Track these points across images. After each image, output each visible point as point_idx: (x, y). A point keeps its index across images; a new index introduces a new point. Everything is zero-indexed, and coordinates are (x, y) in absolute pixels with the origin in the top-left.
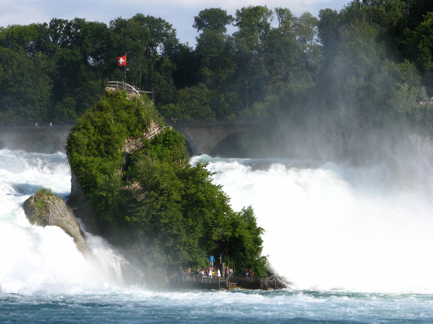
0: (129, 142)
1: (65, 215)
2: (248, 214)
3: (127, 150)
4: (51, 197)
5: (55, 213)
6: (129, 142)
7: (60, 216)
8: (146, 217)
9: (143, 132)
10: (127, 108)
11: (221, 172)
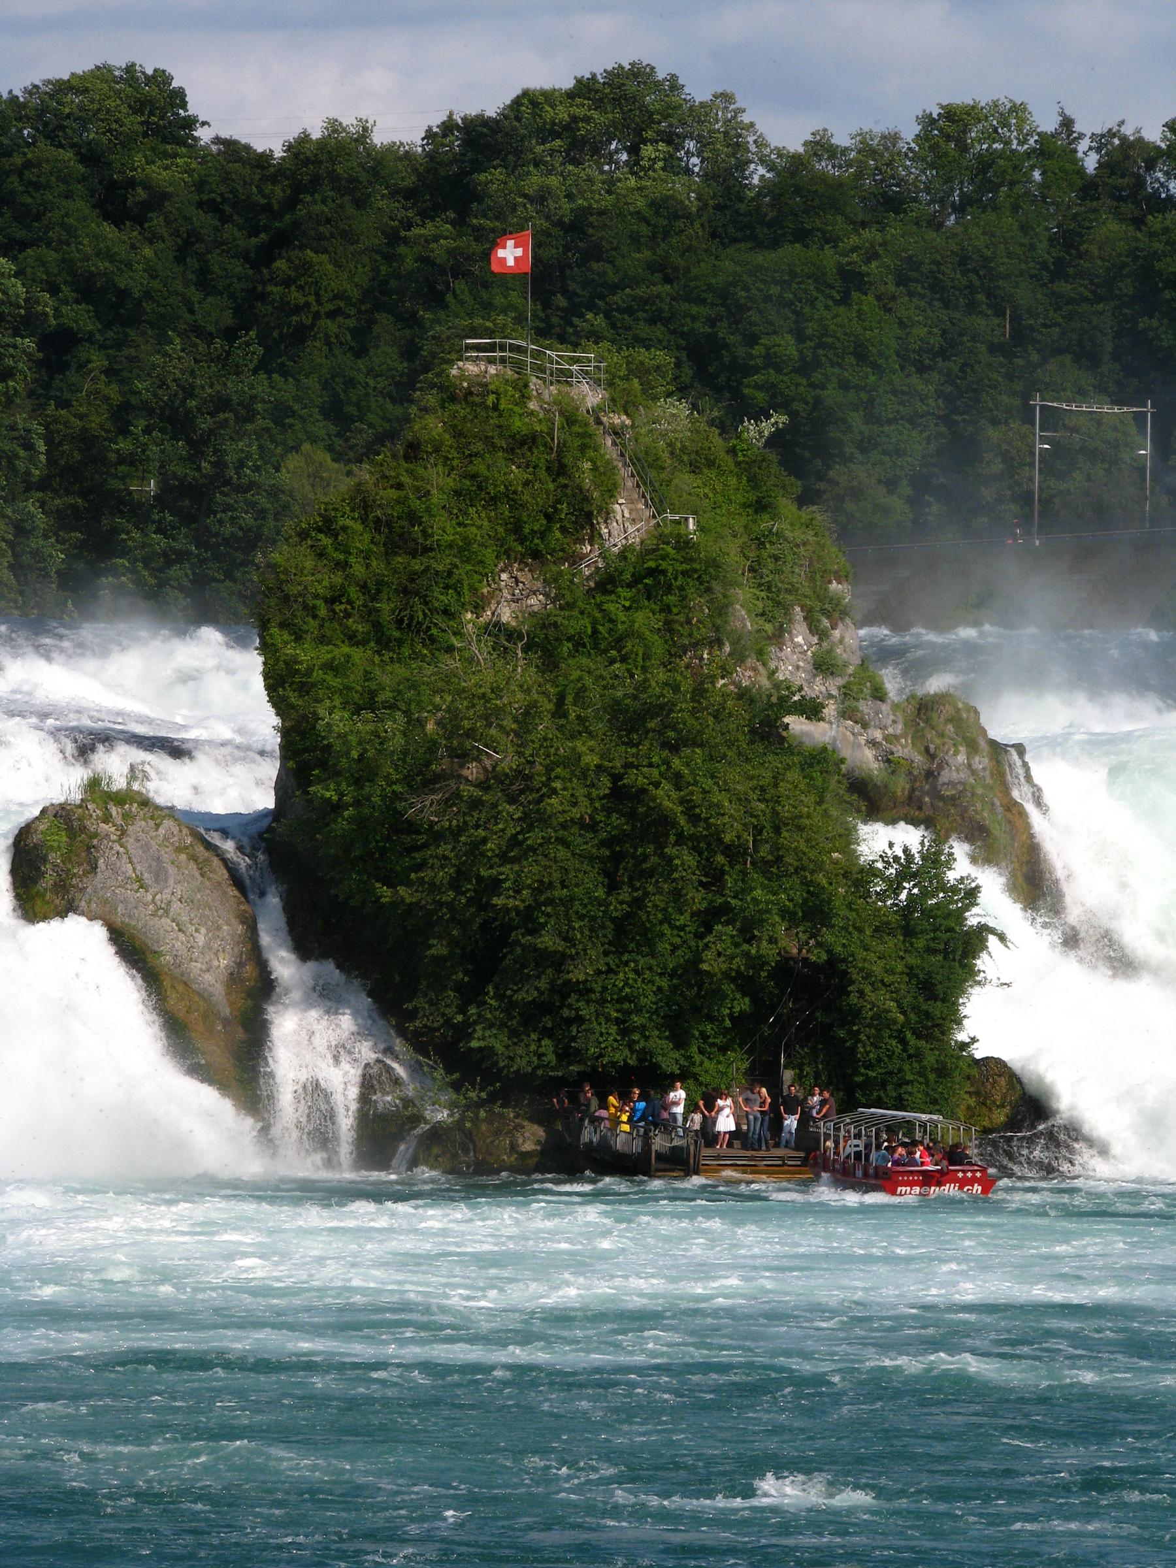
0: (517, 581)
1: (157, 881)
2: (673, 78)
3: (506, 615)
4: (114, 810)
5: (115, 872)
6: (517, 581)
7: (136, 886)
8: (455, 884)
9: (581, 541)
10: (523, 444)
11: (1121, 962)
